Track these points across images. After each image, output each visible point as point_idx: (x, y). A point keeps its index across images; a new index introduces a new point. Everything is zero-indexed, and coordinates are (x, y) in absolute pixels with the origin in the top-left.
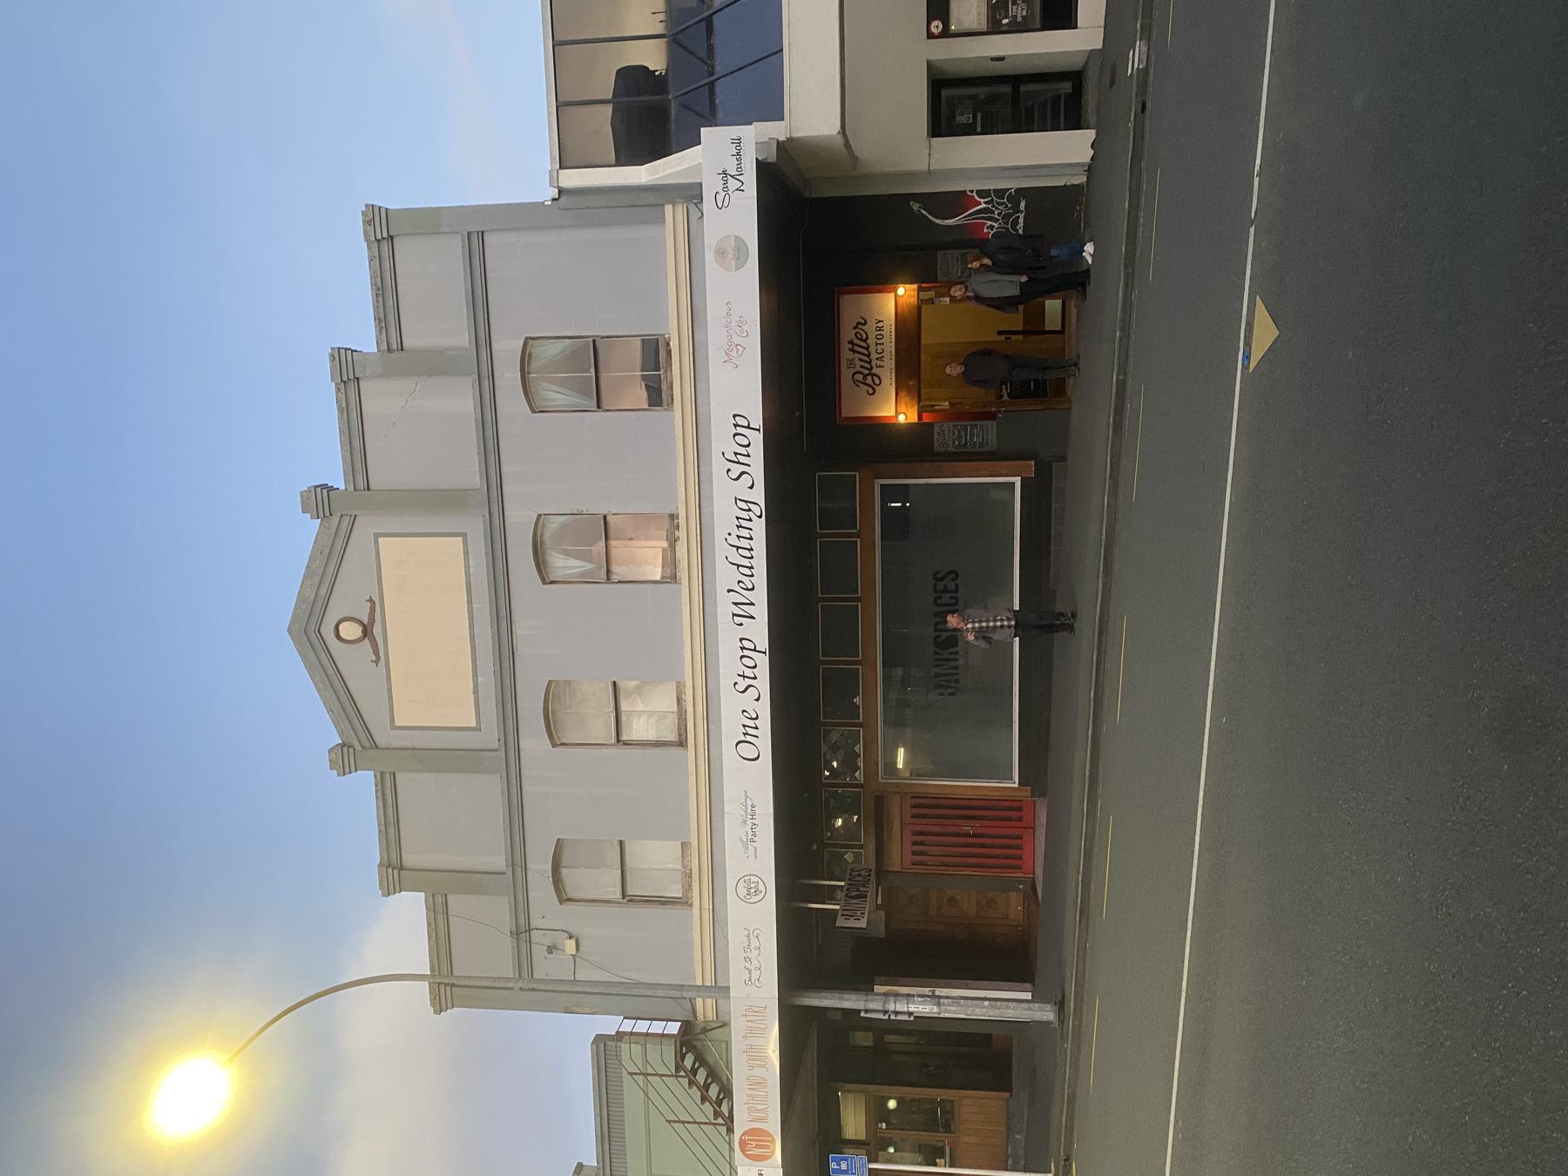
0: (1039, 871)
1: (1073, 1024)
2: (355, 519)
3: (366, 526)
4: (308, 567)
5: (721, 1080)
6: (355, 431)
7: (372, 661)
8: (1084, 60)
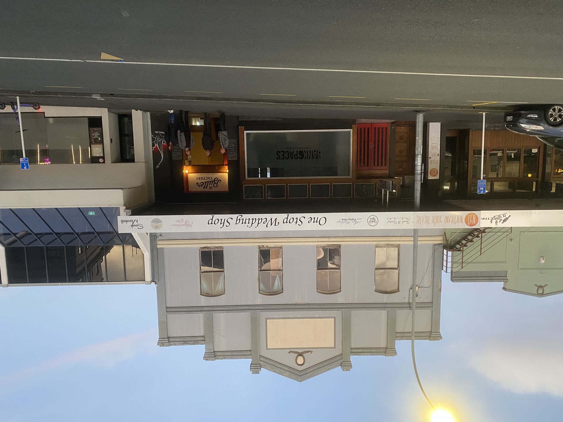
0: (387, 121)
1: (421, 107)
2: (261, 356)
3: (264, 353)
4: (278, 373)
5: (466, 235)
6: (232, 354)
7: (311, 353)
8: (112, 114)
